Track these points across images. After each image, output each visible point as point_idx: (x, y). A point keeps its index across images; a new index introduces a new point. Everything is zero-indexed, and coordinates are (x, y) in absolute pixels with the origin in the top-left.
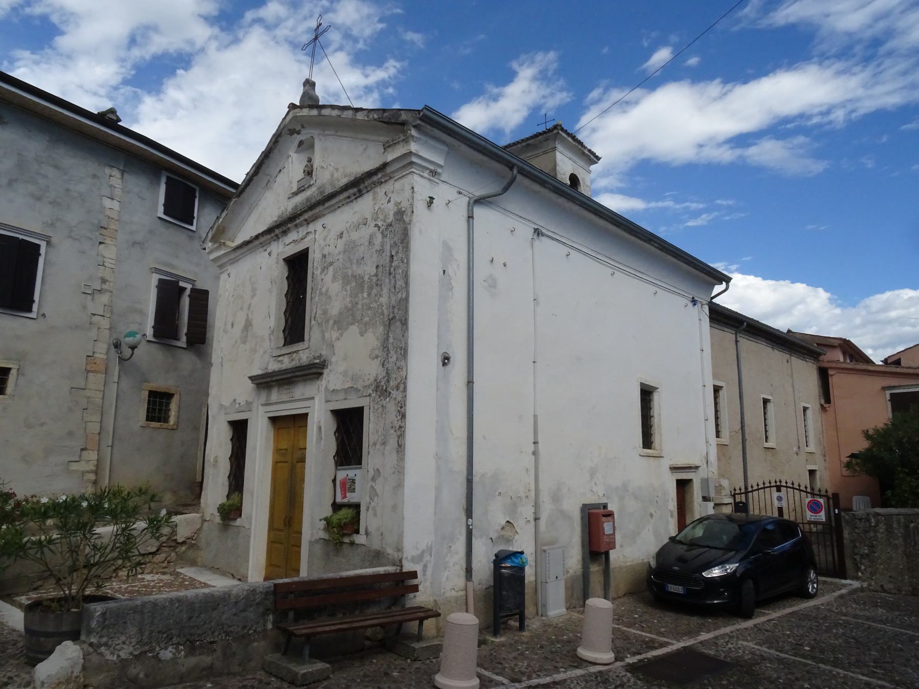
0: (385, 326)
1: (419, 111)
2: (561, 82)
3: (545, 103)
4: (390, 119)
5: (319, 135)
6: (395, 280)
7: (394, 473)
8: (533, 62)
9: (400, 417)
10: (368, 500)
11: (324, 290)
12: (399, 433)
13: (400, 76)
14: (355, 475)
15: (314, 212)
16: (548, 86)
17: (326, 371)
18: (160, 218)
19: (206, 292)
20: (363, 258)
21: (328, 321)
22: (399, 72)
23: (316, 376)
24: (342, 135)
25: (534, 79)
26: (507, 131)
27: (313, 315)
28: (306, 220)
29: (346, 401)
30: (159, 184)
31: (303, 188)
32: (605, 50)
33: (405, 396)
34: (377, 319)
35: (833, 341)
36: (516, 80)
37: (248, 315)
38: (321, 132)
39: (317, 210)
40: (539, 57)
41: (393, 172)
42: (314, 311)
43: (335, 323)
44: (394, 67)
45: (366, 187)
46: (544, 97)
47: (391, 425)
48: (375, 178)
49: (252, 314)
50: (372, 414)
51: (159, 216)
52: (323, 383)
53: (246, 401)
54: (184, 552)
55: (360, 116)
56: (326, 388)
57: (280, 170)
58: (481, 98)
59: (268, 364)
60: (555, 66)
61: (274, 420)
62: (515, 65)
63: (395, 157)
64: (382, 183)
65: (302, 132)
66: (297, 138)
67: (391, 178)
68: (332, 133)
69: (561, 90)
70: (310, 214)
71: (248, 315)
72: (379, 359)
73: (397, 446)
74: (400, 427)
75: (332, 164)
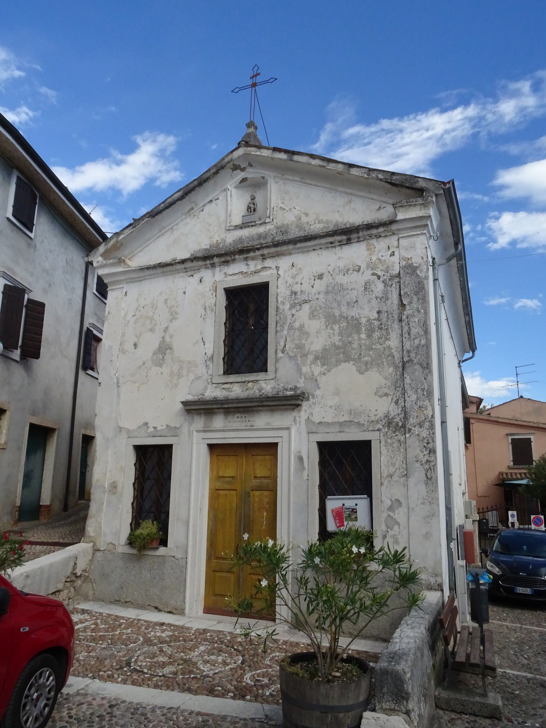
0: (396, 367)
1: (444, 184)
2: (176, 163)
3: (160, 177)
4: (403, 182)
5: (275, 177)
6: (409, 327)
7: (423, 503)
8: (154, 141)
9: (428, 452)
10: (384, 528)
11: (297, 325)
12: (427, 467)
13: (31, 123)
14: (356, 505)
15: (279, 249)
16: (164, 164)
17: (305, 404)
18: (8, 219)
19: (42, 305)
20: (357, 301)
21: (305, 355)
22: (31, 119)
23: (292, 407)
24: (318, 184)
25: (154, 155)
26: (125, 193)
27: (280, 347)
28: (263, 255)
29: (342, 433)
30: (9, 183)
31: (253, 224)
32: (214, 147)
33: (433, 433)
34: (385, 360)
35: (473, 399)
36: (138, 151)
37: (163, 338)
38: (280, 176)
39: (284, 248)
40: (161, 138)
41: (399, 230)
42: (282, 344)
43: (316, 358)
44: (27, 114)
45: (359, 238)
46: (160, 171)
47: (415, 459)
48: (374, 231)
49: (171, 337)
50: (383, 448)
51: (7, 216)
52: (303, 414)
53: (167, 426)
54: (80, 586)
55: (354, 171)
56: (308, 420)
57: (211, 201)
58: (105, 160)
59: (206, 388)
60: (172, 149)
61: (212, 447)
62: (139, 140)
63: (408, 216)
64: (380, 236)
65: (247, 170)
66: (241, 175)
67: (394, 234)
68: (298, 179)
69: (176, 169)
70: (273, 250)
71: (163, 338)
72: (390, 397)
73: (426, 479)
74: (428, 461)
75: (298, 208)
